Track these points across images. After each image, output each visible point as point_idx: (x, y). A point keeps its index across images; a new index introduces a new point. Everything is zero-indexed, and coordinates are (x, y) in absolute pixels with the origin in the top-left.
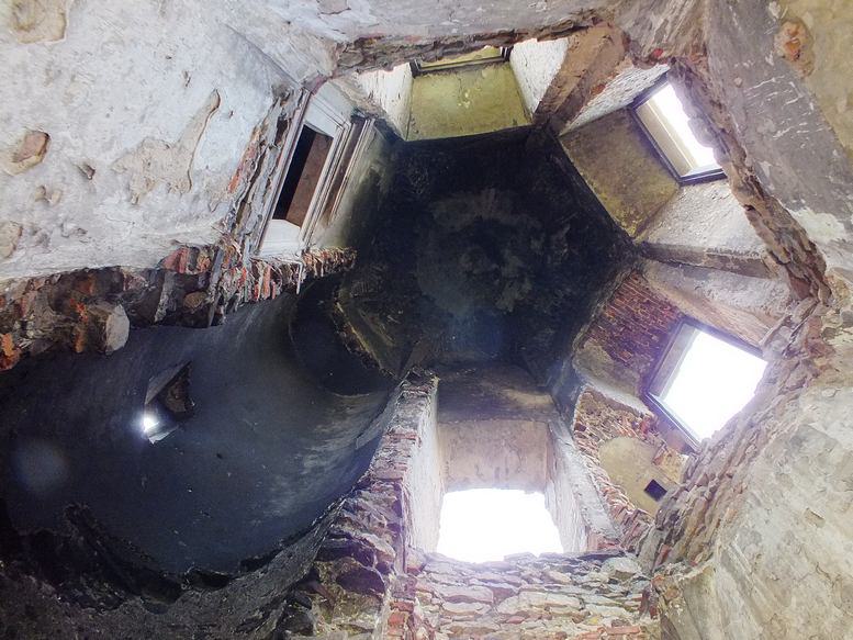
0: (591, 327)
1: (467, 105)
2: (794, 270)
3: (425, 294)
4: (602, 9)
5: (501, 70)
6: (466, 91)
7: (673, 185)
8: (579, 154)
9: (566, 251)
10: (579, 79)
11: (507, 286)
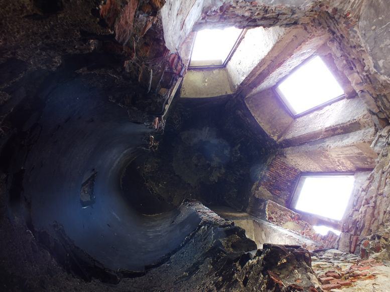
1: (206, 84)
2: (379, 116)
3: (176, 174)
5: (222, 71)
6: (206, 79)
7: (291, 119)
8: (252, 107)
9: (239, 155)
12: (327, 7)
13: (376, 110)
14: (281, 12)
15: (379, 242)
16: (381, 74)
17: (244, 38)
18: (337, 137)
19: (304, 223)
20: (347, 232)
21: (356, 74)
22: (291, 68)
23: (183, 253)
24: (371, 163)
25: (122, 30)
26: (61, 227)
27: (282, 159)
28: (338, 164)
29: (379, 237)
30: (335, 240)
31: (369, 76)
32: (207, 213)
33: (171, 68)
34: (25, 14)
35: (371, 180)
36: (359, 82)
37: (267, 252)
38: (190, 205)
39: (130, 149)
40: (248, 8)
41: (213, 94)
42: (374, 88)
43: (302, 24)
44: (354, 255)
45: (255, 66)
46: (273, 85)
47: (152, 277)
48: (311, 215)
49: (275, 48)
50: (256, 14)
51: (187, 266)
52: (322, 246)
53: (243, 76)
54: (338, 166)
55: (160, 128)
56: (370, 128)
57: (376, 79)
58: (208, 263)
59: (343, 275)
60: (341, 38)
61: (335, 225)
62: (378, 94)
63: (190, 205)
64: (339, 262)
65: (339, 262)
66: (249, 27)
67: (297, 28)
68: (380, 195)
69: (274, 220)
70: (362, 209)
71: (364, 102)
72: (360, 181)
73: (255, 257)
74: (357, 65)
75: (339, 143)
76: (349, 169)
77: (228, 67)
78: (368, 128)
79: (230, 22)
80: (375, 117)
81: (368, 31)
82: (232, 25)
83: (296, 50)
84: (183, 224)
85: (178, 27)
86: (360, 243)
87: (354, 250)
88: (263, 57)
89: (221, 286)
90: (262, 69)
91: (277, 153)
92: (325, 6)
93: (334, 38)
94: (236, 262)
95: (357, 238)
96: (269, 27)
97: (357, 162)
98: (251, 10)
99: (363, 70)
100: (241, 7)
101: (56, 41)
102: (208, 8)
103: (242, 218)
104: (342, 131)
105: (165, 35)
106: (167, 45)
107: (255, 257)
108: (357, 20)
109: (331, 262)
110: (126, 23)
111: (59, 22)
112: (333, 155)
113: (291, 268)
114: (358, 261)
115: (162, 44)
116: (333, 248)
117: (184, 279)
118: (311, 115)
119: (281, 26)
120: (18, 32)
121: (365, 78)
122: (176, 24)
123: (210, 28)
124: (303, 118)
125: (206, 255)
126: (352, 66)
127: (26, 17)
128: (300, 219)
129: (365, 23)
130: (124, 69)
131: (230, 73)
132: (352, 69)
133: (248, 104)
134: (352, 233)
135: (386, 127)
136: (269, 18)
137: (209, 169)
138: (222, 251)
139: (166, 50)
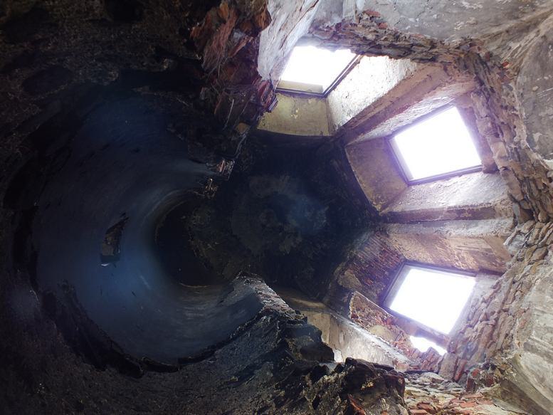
0: (347, 265)
1: (296, 116)
2: (522, 205)
4: (478, 40)
7: (404, 185)
9: (325, 221)
10: (390, 103)
11: (287, 237)
12: (479, 49)
13: (519, 197)
14: (417, 42)
15: (493, 374)
16: (535, 151)
17: (359, 63)
18: (463, 223)
19: (398, 329)
20: (454, 353)
21: (501, 145)
22: (417, 116)
23: (233, 349)
24: (501, 265)
25: (212, 56)
26: (72, 289)
27: (383, 238)
28: (457, 258)
29: (494, 367)
30: (435, 361)
31: (519, 150)
32: (272, 299)
33: (258, 99)
34: (91, 18)
35: (497, 288)
36: (503, 155)
37: (350, 369)
38: (248, 282)
39: (177, 191)
40: (373, 29)
41: (302, 131)
42: (522, 168)
43: (442, 62)
44: (458, 385)
45: (368, 105)
46: (388, 134)
47: (187, 375)
48: (409, 321)
49: (400, 87)
50: (382, 39)
51: (238, 368)
52: (418, 366)
53: (349, 114)
54: (457, 261)
55: (226, 171)
56: (507, 219)
57: (526, 156)
58: (267, 369)
59: (439, 409)
60: (490, 92)
61: (440, 340)
62: (526, 176)
63: (248, 282)
64: (437, 391)
65: (437, 391)
66: (370, 53)
67: (435, 66)
68: (505, 311)
69: (360, 319)
70: (479, 326)
71: (505, 183)
72: (482, 286)
73: (333, 374)
74: (505, 133)
75: (463, 231)
76: (471, 268)
77: (329, 97)
78: (505, 218)
79: (346, 43)
80: (516, 206)
81: (528, 90)
82: (348, 47)
83: (427, 95)
84: (236, 307)
85: (277, 45)
86: (468, 371)
87: (459, 378)
88: (381, 95)
89: (282, 404)
90: (377, 110)
91: (377, 228)
92: (476, 47)
93: (481, 90)
94: (306, 374)
95: (466, 363)
96: (397, 59)
97: (483, 261)
98: (377, 32)
99: (512, 141)
100: (363, 26)
101: (119, 53)
102: (320, 21)
103: (316, 310)
104: (470, 215)
105: (259, 56)
106: (259, 69)
107: (333, 373)
108: (516, 74)
109: (426, 390)
110: (219, 46)
111: (132, 33)
112: (453, 245)
113: (378, 394)
114: (462, 395)
115: (253, 67)
116: (432, 371)
117: (232, 385)
118: (432, 185)
119: (413, 60)
120: (75, 37)
121: (513, 151)
122: (275, 43)
123: (317, 46)
124: (420, 186)
125: (265, 358)
126: (499, 132)
127: (90, 21)
128: (394, 325)
129: (525, 80)
130: (198, 96)
131: (332, 107)
132: (497, 136)
133: (349, 154)
134: (460, 355)
135: (529, 222)
136: (400, 48)
137: (281, 234)
138: (288, 355)
139: (257, 76)
